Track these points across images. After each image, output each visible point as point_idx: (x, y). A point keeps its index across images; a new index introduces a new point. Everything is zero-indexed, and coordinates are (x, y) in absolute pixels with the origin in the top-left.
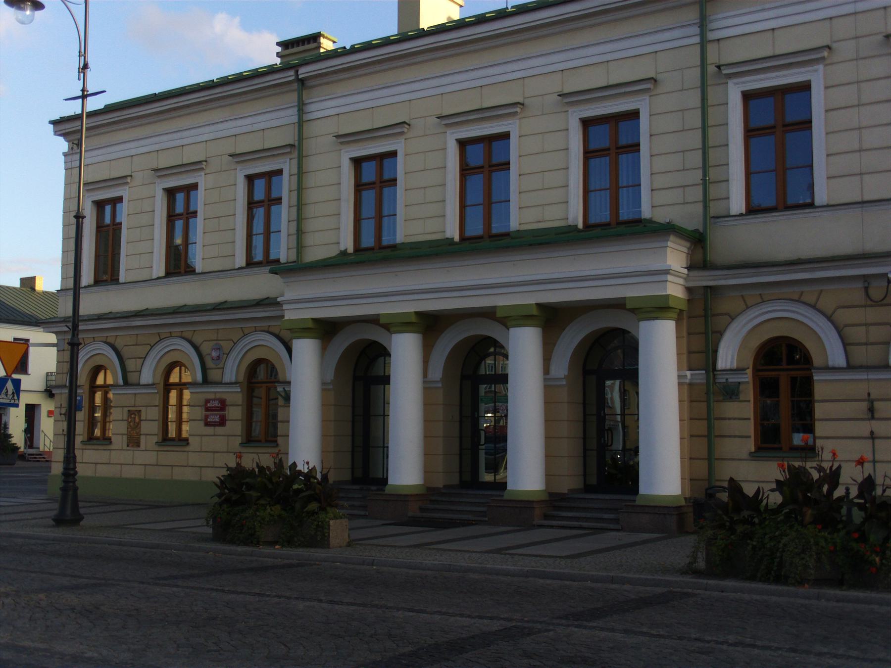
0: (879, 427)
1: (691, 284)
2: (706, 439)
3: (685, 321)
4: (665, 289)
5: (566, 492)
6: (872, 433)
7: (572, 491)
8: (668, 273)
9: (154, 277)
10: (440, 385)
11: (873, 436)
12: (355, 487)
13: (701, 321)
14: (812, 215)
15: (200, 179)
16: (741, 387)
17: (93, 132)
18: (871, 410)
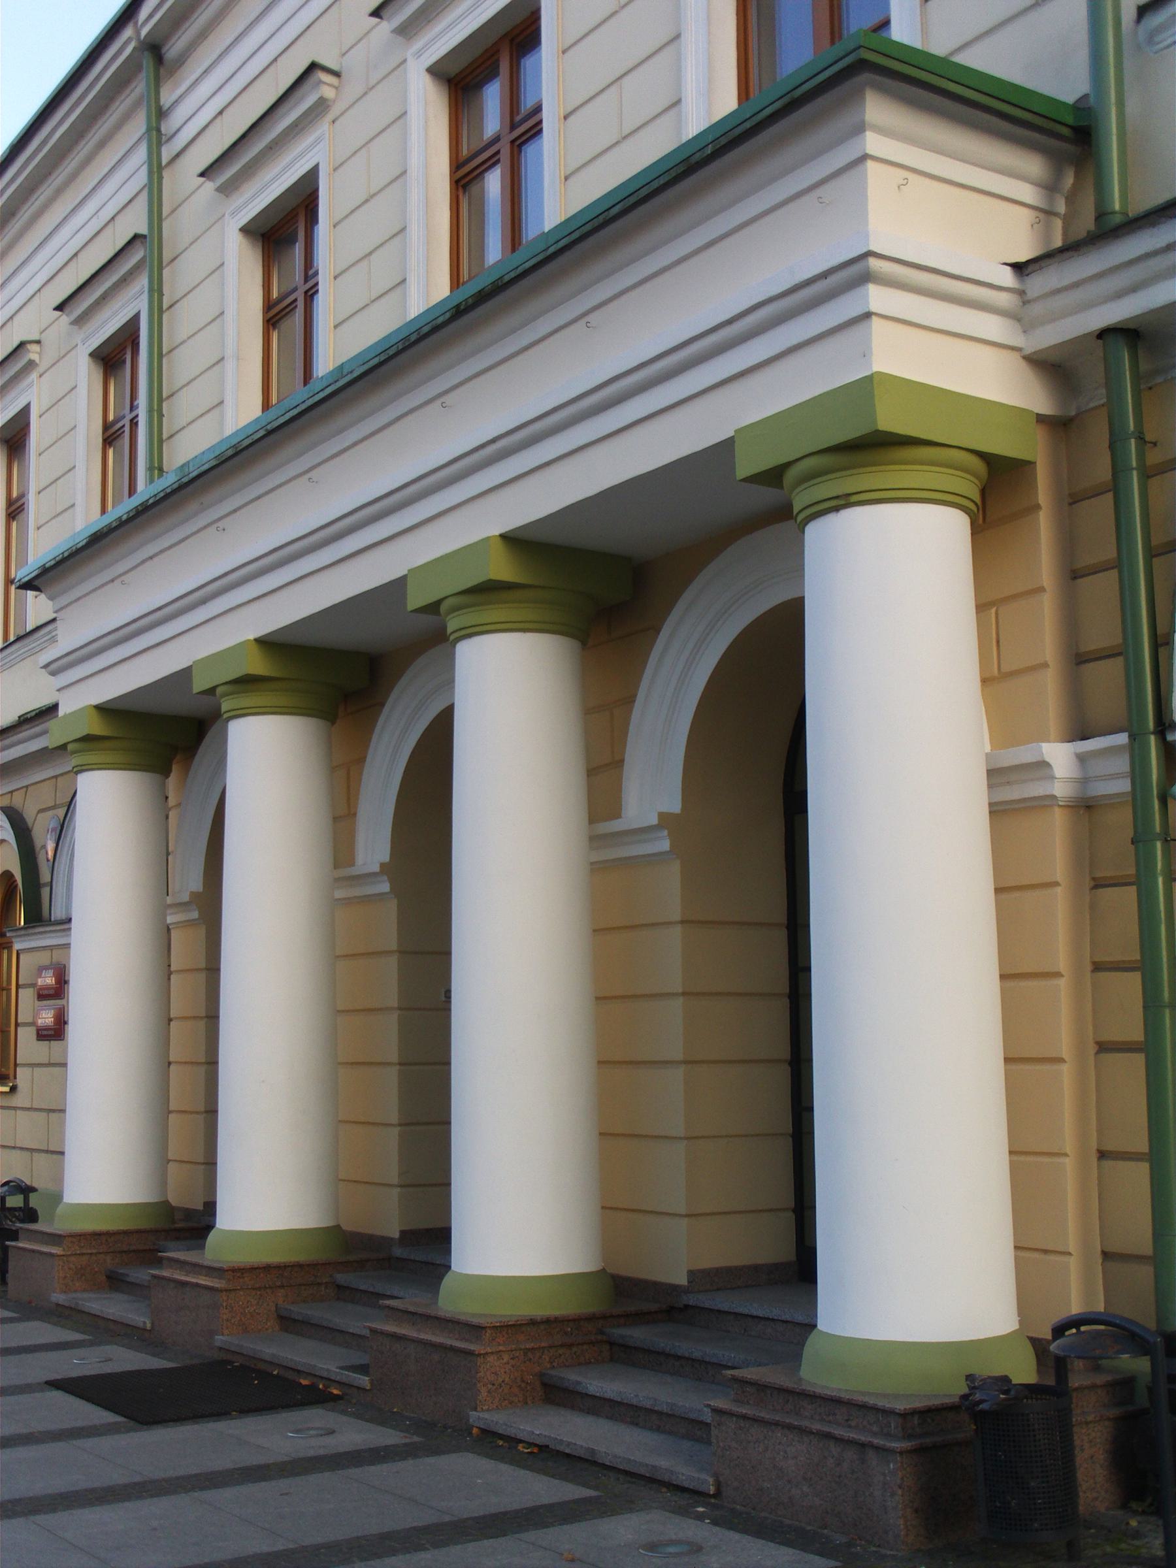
1: (1049, 337)
2: (1139, 1059)
4: (866, 355)
5: (682, 1280)
7: (704, 1279)
8: (866, 278)
10: (385, 887)
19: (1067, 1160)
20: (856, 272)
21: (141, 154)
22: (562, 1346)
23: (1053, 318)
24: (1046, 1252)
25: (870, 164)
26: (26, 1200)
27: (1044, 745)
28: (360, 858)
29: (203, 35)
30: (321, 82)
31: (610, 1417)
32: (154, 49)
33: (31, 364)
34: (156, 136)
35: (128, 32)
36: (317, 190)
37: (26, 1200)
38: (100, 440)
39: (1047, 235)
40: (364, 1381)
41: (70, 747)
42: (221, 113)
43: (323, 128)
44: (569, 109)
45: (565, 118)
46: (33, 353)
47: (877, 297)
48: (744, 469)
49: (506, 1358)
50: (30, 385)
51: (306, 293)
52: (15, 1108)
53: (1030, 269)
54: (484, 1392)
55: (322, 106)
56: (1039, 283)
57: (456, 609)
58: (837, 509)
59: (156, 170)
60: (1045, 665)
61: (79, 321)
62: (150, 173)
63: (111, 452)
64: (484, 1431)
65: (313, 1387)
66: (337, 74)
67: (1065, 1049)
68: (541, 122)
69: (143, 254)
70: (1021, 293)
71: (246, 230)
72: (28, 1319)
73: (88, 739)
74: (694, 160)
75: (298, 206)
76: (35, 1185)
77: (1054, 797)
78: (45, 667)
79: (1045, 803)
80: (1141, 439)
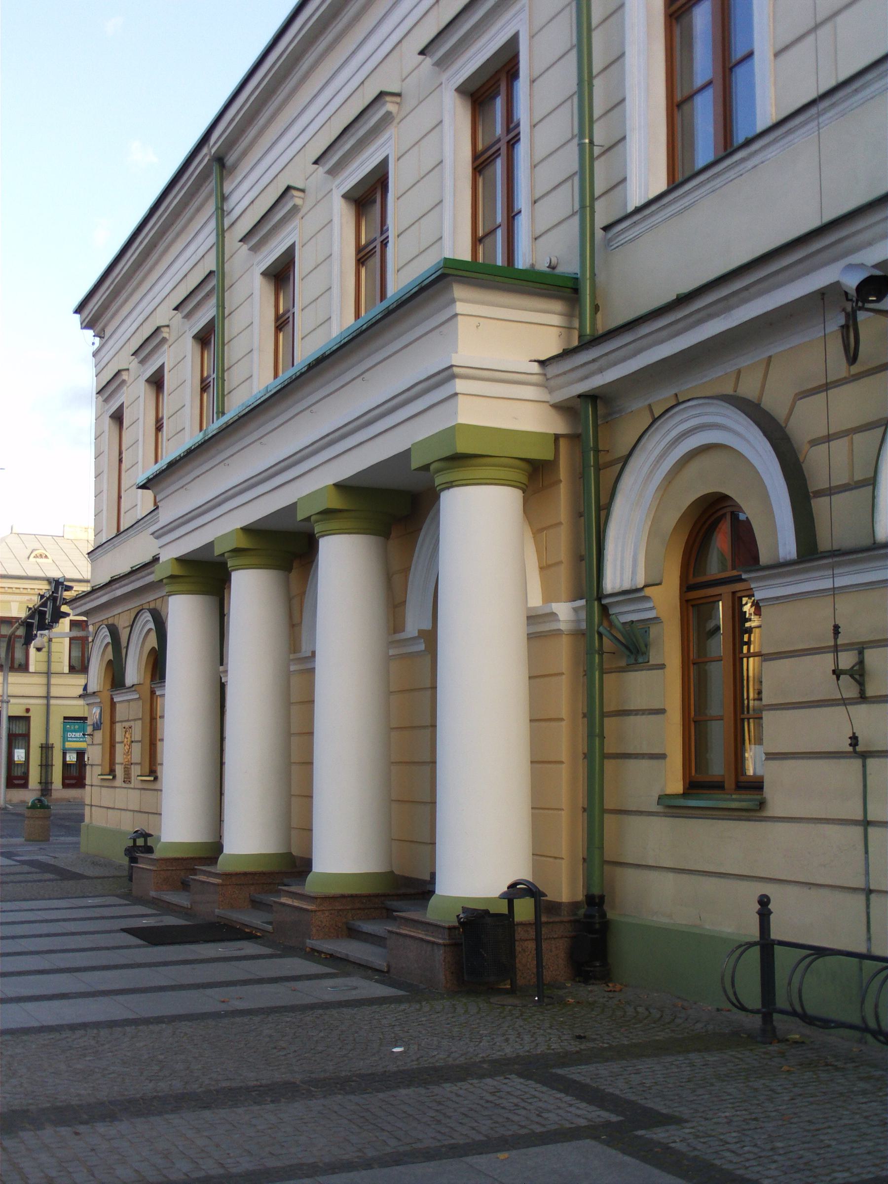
0: (878, 725)
6: (854, 740)
8: (454, 376)
11: (858, 750)
12: (31, 848)
13: (569, 473)
14: (750, 164)
16: (653, 631)
19: (563, 812)
20: (447, 375)
21: (212, 224)
22: (359, 909)
23: (561, 387)
24: (555, 858)
25: (459, 317)
26: (146, 841)
27: (553, 604)
28: (304, 648)
29: (244, 154)
30: (293, 196)
31: (372, 943)
32: (220, 160)
33: (164, 340)
34: (221, 213)
35: (205, 150)
36: (388, 173)
37: (146, 841)
38: (199, 389)
39: (569, 339)
40: (270, 928)
41: (164, 581)
42: (252, 202)
43: (296, 222)
44: (400, 231)
45: (398, 236)
46: (165, 333)
47: (460, 385)
48: (415, 465)
49: (327, 913)
50: (164, 352)
51: (508, 142)
52: (115, 787)
53: (548, 363)
54: (314, 930)
55: (295, 209)
56: (552, 370)
57: (438, 471)
58: (448, 488)
59: (221, 233)
60: (561, 562)
61: (188, 316)
62: (217, 235)
63: (205, 396)
64: (313, 950)
65: (251, 933)
66: (303, 191)
67: (564, 756)
68: (519, 134)
69: (214, 284)
70: (545, 375)
71: (265, 274)
72: (134, 904)
73: (172, 577)
74: (391, 308)
75: (498, 72)
76: (151, 832)
77: (559, 630)
78: (152, 534)
79: (558, 633)
80: (597, 451)
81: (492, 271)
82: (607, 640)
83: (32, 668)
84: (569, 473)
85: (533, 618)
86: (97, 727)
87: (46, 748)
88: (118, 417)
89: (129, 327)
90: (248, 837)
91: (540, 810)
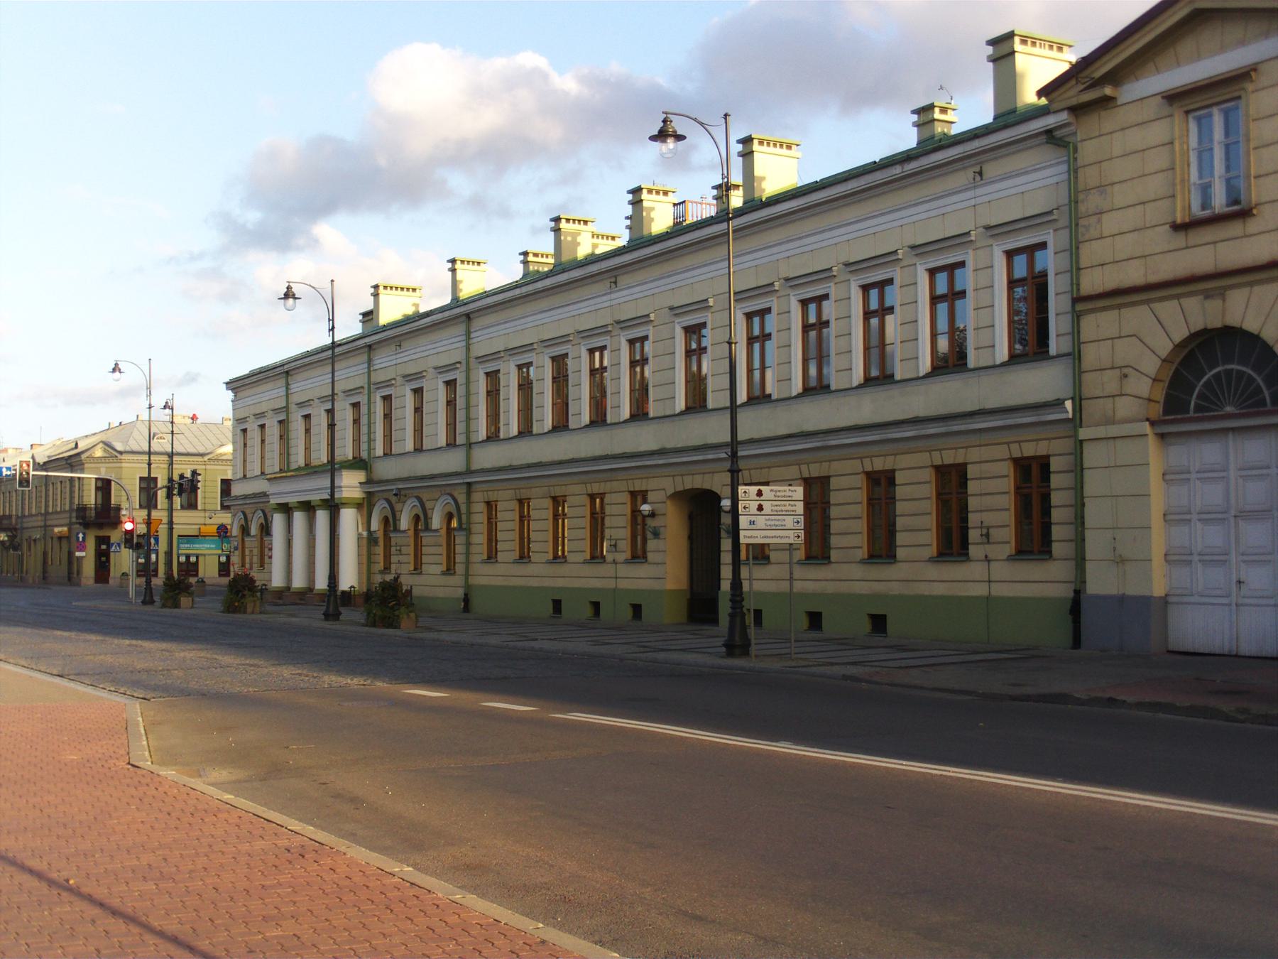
3: (974, 454)
9: (998, 362)
13: (366, 506)
15: (650, 331)
17: (741, 233)
18: (987, 535)
81: (358, 463)
82: (372, 540)
83: (1053, 350)
84: (366, 506)
85: (359, 534)
86: (236, 549)
87: (169, 554)
88: (244, 431)
89: (249, 401)
90: (298, 582)
91: (360, 573)
